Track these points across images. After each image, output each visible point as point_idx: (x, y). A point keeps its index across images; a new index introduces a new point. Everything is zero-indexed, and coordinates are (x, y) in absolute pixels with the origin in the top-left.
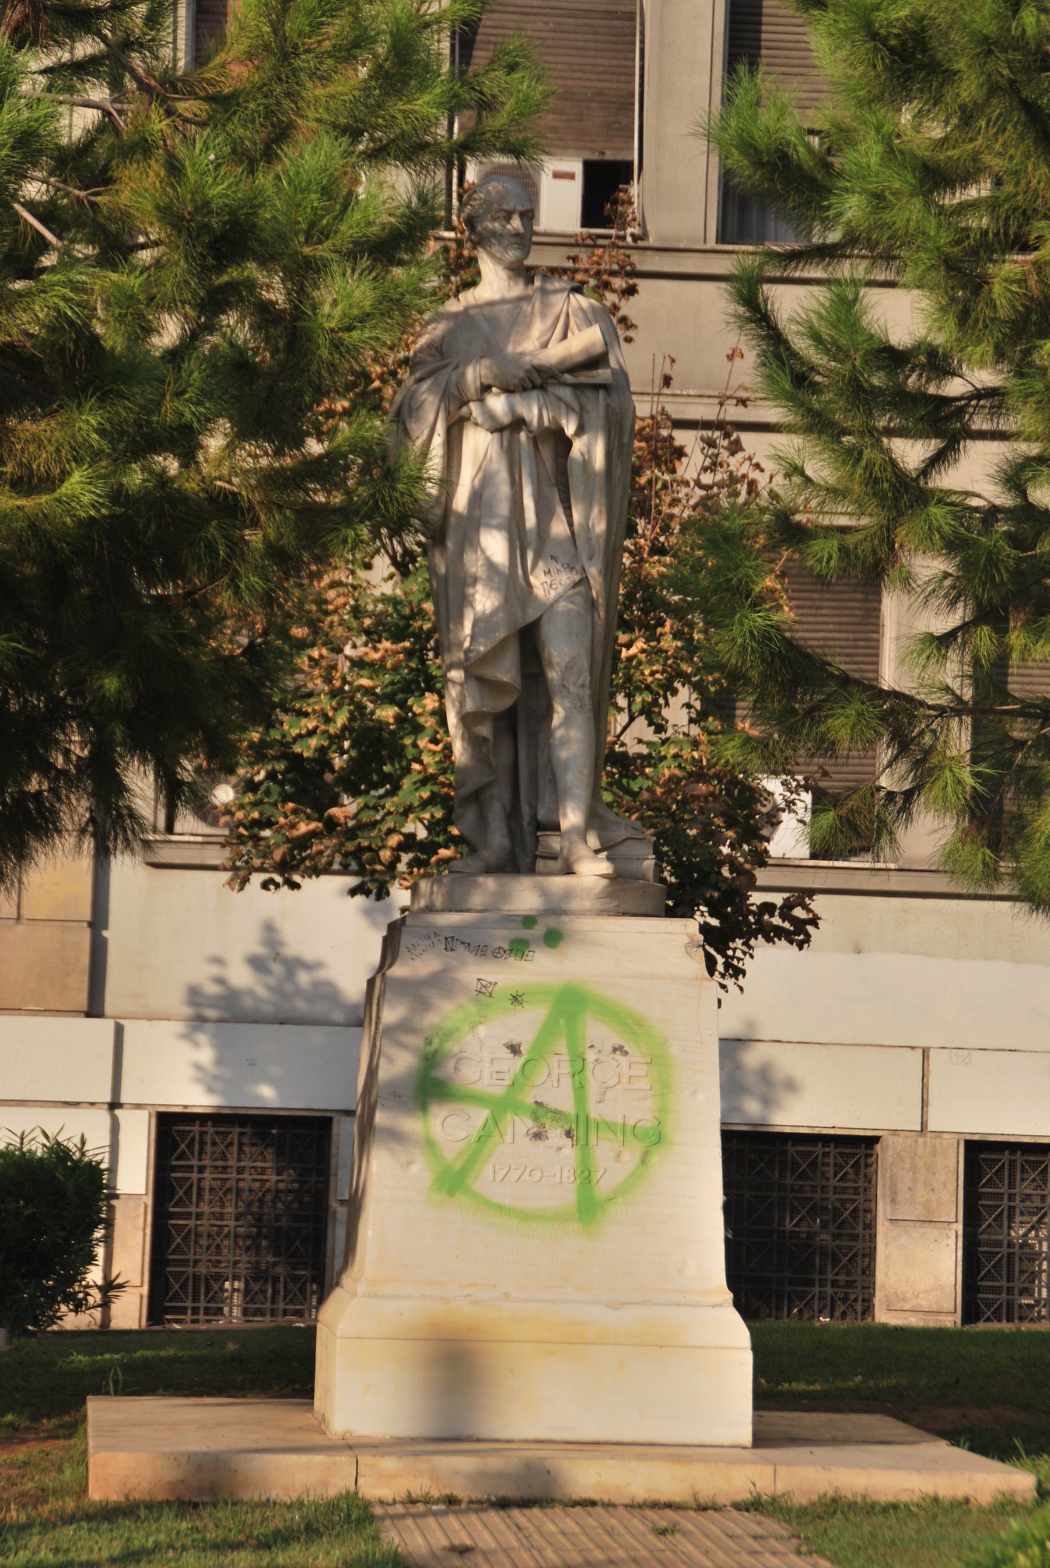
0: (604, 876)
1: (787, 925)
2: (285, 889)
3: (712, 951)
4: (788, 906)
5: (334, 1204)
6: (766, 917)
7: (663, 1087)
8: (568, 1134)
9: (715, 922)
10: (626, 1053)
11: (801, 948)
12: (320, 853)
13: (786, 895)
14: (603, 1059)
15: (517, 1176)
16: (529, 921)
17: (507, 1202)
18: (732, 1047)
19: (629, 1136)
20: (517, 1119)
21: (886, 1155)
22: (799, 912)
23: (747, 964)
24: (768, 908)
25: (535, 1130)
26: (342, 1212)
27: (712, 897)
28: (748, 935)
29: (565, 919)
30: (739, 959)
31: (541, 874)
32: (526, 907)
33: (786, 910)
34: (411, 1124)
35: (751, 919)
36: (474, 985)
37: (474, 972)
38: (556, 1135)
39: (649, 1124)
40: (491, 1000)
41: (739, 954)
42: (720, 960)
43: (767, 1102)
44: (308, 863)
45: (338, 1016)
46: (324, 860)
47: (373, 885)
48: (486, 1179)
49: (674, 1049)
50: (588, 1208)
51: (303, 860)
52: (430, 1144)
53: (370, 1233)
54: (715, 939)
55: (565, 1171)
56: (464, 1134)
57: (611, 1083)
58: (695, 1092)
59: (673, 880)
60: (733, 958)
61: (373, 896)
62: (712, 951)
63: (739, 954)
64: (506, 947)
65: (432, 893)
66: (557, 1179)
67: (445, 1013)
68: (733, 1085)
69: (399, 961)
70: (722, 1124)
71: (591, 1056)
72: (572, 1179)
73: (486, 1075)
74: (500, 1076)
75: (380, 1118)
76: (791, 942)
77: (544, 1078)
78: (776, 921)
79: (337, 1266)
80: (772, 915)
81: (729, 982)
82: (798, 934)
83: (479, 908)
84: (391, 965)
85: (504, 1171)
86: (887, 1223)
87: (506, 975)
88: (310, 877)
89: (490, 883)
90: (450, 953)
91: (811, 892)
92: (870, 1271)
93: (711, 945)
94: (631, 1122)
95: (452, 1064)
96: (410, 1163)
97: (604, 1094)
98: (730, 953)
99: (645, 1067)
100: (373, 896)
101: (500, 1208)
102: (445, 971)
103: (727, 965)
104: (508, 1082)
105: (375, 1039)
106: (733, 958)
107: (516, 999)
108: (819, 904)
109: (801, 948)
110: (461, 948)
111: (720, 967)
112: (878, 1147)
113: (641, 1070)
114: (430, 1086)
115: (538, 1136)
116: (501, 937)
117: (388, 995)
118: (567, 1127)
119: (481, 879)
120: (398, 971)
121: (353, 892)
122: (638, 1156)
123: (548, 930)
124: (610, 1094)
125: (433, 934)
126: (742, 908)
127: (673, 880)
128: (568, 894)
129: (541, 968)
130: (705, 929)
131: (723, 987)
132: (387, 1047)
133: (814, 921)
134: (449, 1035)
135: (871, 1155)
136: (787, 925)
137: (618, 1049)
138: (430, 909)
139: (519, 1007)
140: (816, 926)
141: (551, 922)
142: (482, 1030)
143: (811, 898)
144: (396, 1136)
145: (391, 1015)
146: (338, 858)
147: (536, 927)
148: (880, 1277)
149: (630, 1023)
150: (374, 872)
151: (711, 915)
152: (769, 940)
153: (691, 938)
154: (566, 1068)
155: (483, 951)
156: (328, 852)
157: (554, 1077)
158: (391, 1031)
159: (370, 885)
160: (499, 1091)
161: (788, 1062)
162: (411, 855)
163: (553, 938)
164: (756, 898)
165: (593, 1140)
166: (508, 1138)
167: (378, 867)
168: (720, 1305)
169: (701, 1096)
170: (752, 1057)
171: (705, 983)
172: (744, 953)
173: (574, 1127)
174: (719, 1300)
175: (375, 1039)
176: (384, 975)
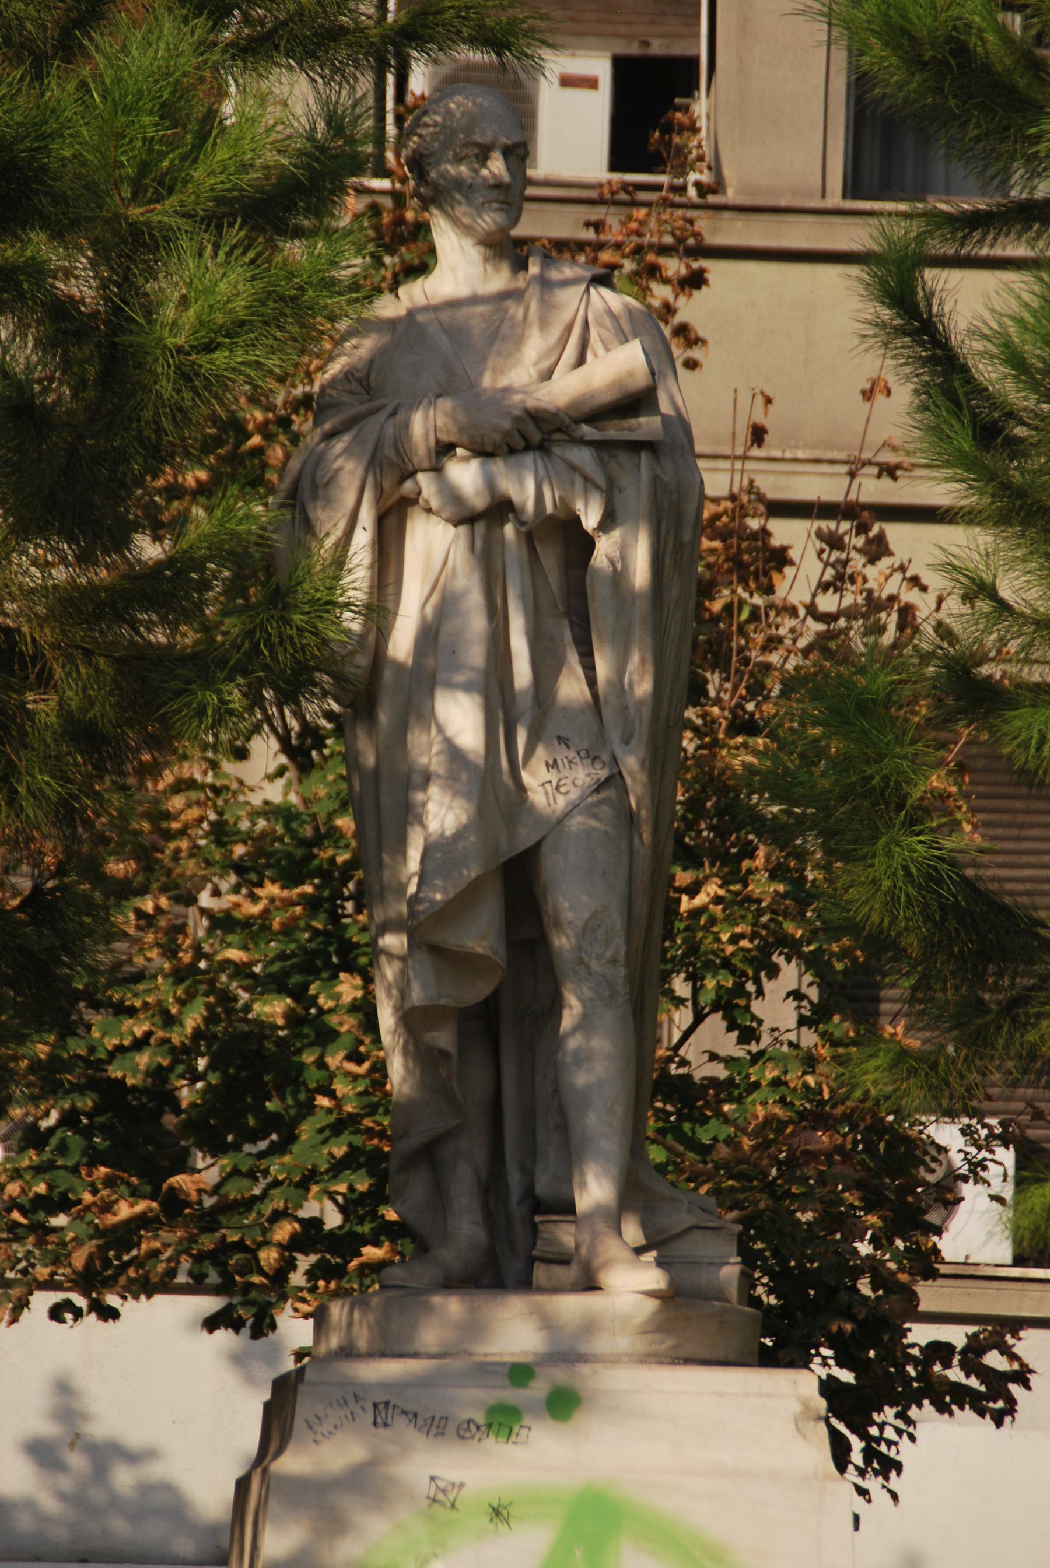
0: (651, 1294)
1: (974, 1382)
4: (975, 1349)
6: (937, 1368)
9: (846, 1376)
11: (999, 1424)
13: (971, 1329)
16: (520, 1373)
22: (994, 1360)
23: (905, 1452)
24: (940, 1351)
27: (840, 1330)
28: (905, 1400)
29: (584, 1369)
30: (890, 1443)
31: (542, 1290)
33: (971, 1357)
35: (911, 1370)
36: (424, 1487)
37: (423, 1464)
41: (890, 1433)
42: (857, 1444)
44: (132, 1273)
46: (161, 1267)
47: (247, 1313)
51: (124, 1266)
54: (849, 1407)
59: (773, 1300)
60: (878, 1440)
61: (246, 1331)
64: (480, 1419)
65: (350, 1324)
76: (981, 1413)
78: (955, 1374)
80: (947, 1365)
81: (873, 1484)
83: (434, 1350)
84: (279, 1453)
89: (453, 1306)
90: (382, 1431)
91: (1017, 1325)
93: (840, 1418)
98: (874, 1431)
100: (246, 1331)
103: (869, 1454)
106: (878, 1440)
109: (999, 1424)
110: (401, 1423)
111: (857, 1457)
116: (471, 1402)
117: (272, 1503)
119: (437, 1300)
120: (291, 1463)
121: (211, 1324)
123: (553, 1390)
125: (354, 1395)
126: (895, 1351)
127: (773, 1300)
128: (590, 1326)
129: (541, 1457)
130: (829, 1388)
131: (862, 1492)
133: (1022, 1377)
136: (974, 1382)
138: (348, 1352)
139: (503, 1528)
140: (1027, 1386)
141: (559, 1375)
143: (1015, 1334)
151: (840, 1365)
152: (943, 1409)
153: (806, 1405)
155: (439, 1426)
156: (167, 1254)
162: (313, 1258)
163: (563, 1404)
164: (920, 1334)
167: (257, 1279)
172: (899, 1432)
176: (265, 1471)
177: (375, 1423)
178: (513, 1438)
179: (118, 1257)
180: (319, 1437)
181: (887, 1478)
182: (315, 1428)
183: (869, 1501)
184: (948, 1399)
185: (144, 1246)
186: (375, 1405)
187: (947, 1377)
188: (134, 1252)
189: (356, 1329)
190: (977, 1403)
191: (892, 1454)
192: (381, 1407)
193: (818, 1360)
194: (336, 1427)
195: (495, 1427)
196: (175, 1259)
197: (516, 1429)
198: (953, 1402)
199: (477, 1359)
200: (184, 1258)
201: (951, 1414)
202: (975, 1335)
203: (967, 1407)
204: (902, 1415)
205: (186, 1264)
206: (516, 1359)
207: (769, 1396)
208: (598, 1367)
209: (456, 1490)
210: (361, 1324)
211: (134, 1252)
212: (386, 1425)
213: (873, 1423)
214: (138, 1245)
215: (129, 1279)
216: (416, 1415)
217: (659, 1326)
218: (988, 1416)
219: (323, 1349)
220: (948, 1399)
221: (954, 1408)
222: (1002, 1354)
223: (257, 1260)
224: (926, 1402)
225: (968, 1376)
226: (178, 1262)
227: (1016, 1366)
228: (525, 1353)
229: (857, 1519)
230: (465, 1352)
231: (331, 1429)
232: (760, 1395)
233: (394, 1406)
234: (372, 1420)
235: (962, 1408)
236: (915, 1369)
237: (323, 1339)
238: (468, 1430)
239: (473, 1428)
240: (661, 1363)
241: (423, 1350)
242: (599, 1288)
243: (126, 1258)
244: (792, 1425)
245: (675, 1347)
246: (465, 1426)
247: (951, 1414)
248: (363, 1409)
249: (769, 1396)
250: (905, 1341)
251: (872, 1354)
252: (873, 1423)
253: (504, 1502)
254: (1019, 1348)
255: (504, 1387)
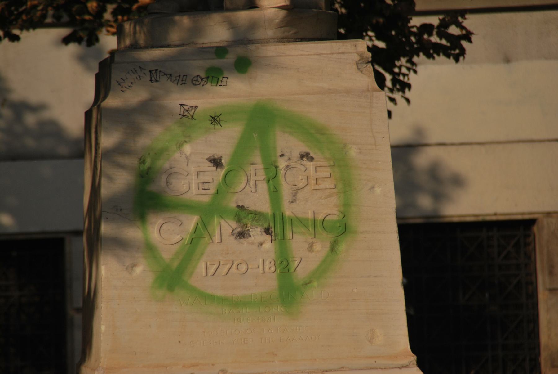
0: (282, 8)
1: (444, 42)
2: (6, 41)
3: (381, 70)
4: (444, 25)
5: (71, 312)
6: (426, 36)
7: (346, 185)
8: (267, 231)
9: (381, 45)
10: (312, 159)
11: (457, 60)
12: (34, 7)
13: (441, 17)
14: (292, 165)
15: (226, 270)
16: (220, 51)
17: (219, 293)
18: (403, 153)
19: (319, 229)
20: (223, 222)
21: (542, 236)
22: (454, 30)
23: (412, 78)
24: (427, 28)
25: (239, 230)
26: (78, 318)
27: (378, 22)
28: (410, 54)
29: (252, 47)
30: (404, 75)
31: (228, 10)
32: (217, 40)
33: (442, 30)
34: (133, 233)
35: (413, 39)
36: (178, 110)
37: (178, 98)
38: (257, 234)
39: (335, 218)
40: (193, 122)
41: (404, 70)
42: (388, 77)
43: (438, 196)
44: (24, 17)
45: (63, 150)
46: (38, 14)
47: (83, 34)
48: (200, 274)
49: (353, 152)
50: (289, 292)
51: (20, 14)
52: (150, 248)
53: (103, 328)
54: (382, 60)
55: (267, 263)
56: (178, 238)
57: (301, 185)
58: (373, 188)
59: (344, 11)
60: (399, 74)
61: (84, 43)
62: (381, 70)
63: (404, 70)
64: (203, 75)
65: (135, 33)
66: (261, 270)
67: (155, 135)
68: (405, 185)
69: (111, 93)
70: (398, 218)
71: (282, 164)
72: (273, 269)
73: (194, 186)
74: (206, 186)
75: (105, 229)
76: (448, 56)
77: (243, 185)
78: (435, 39)
79: (77, 359)
80: (430, 34)
81: (397, 96)
82: (454, 49)
83: (177, 43)
84: (105, 98)
85: (215, 267)
86: (547, 293)
87: (204, 99)
88: (28, 29)
89: (185, 21)
90: (155, 84)
91: (463, 13)
92: (534, 333)
93: (379, 65)
94: (320, 217)
95: (164, 178)
96: (133, 266)
97: (295, 195)
98: (396, 70)
99: (329, 169)
100: (84, 43)
101: (213, 299)
102: (152, 100)
103: (395, 81)
104: (213, 191)
105: (95, 162)
106: (399, 74)
107: (215, 119)
108: (471, 22)
109: (457, 60)
110: (164, 79)
111: (389, 83)
112: (535, 229)
113: (325, 172)
114: (148, 198)
115: (242, 235)
116: (198, 67)
117: (104, 122)
118: (266, 225)
119: (177, 18)
120: (112, 102)
121: (66, 41)
122: (328, 245)
123: (238, 58)
124: (300, 195)
125: (139, 68)
126: (405, 31)
127: (344, 11)
128: (253, 25)
129: (234, 91)
130: (373, 49)
131: (392, 100)
132: (107, 168)
133: (468, 36)
134: (160, 153)
135: (529, 236)
136: (444, 42)
137: (305, 156)
138: (135, 46)
139: (218, 127)
140: (470, 41)
141: (240, 51)
142: (187, 149)
143: (463, 17)
144: (120, 244)
145: (107, 140)
146: (51, 12)
147: (227, 56)
148: (544, 339)
149: (314, 133)
150: (84, 21)
151: (378, 38)
152: (429, 56)
153: (361, 55)
154: (261, 175)
155: (184, 80)
156: (40, 8)
157: (252, 183)
158: (109, 154)
159: (81, 34)
160: (206, 199)
161: (454, 161)
162: (114, 6)
163: (243, 65)
164: (416, 22)
165: (289, 235)
166: (217, 238)
167: (87, 17)
168: (406, 366)
169: (378, 190)
170: (422, 160)
171: (375, 94)
172: (409, 69)
173: (272, 224)
174: (405, 362)
175: (95, 162)
176: (99, 106)
177: (151, 80)
178: (219, 84)
179: (17, 9)
180: (124, 89)
181: (404, 92)
182: (122, 84)
183: (396, 104)
184: (431, 51)
185: (29, 3)
186: (150, 71)
187: (430, 41)
188: (24, 7)
189: (138, 35)
190: (446, 51)
191: (406, 80)
192: (153, 72)
193: (367, 38)
194: (132, 83)
195: (210, 79)
196: (45, 9)
197: (221, 79)
198: (434, 52)
199: (199, 46)
200: (50, 8)
201: (434, 58)
202: (444, 19)
203: (441, 54)
204: (410, 61)
205: (51, 12)
206: (218, 45)
207: (343, 53)
208: (259, 45)
209: (193, 110)
210: (140, 33)
211: (24, 7)
212: (157, 81)
213: (395, 66)
214: (25, 3)
215: (23, 20)
216: (171, 75)
217: (287, 23)
218: (452, 58)
219: (122, 46)
220: (431, 51)
221: (435, 55)
222: (457, 26)
223: (86, 7)
224: (421, 54)
225: (441, 39)
226: (47, 11)
227: (464, 32)
228: (222, 41)
229: (390, 114)
230: (193, 43)
231: (130, 84)
232: (339, 53)
233: (160, 72)
234: (150, 79)
235: (439, 55)
236: (415, 38)
237: (122, 42)
238: (197, 81)
239: (199, 79)
240: (289, 42)
241: (172, 43)
242: (258, 7)
243: (21, 10)
244: (355, 66)
245: (295, 33)
246: (195, 79)
247: (434, 58)
248: (145, 74)
249: (343, 53)
250: (409, 25)
251: (393, 33)
252: (395, 66)
253: (218, 114)
254: (466, 23)
255: (213, 59)
